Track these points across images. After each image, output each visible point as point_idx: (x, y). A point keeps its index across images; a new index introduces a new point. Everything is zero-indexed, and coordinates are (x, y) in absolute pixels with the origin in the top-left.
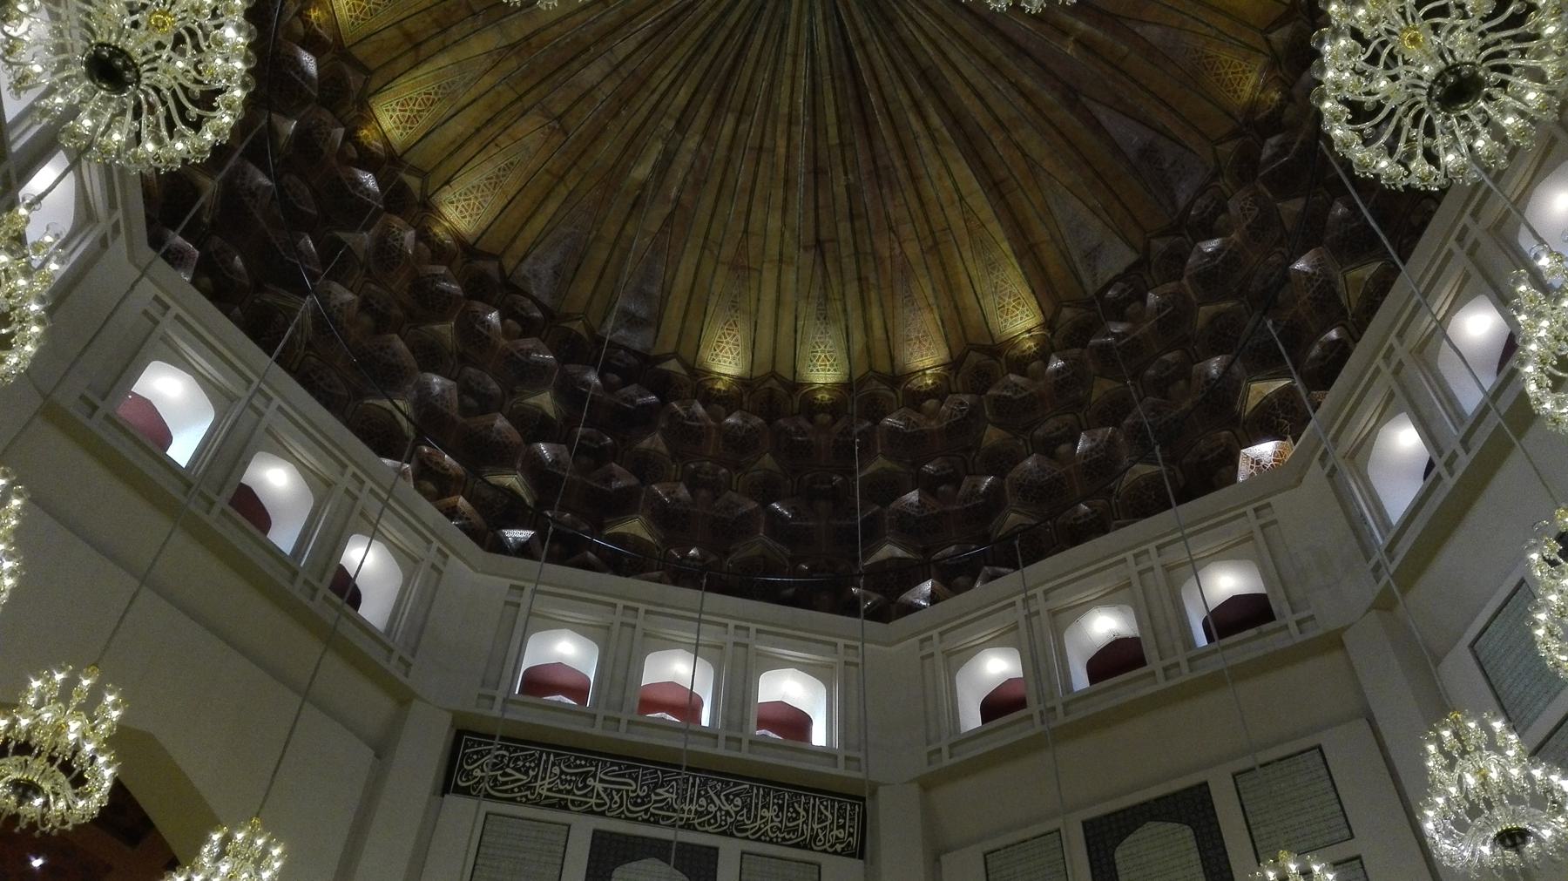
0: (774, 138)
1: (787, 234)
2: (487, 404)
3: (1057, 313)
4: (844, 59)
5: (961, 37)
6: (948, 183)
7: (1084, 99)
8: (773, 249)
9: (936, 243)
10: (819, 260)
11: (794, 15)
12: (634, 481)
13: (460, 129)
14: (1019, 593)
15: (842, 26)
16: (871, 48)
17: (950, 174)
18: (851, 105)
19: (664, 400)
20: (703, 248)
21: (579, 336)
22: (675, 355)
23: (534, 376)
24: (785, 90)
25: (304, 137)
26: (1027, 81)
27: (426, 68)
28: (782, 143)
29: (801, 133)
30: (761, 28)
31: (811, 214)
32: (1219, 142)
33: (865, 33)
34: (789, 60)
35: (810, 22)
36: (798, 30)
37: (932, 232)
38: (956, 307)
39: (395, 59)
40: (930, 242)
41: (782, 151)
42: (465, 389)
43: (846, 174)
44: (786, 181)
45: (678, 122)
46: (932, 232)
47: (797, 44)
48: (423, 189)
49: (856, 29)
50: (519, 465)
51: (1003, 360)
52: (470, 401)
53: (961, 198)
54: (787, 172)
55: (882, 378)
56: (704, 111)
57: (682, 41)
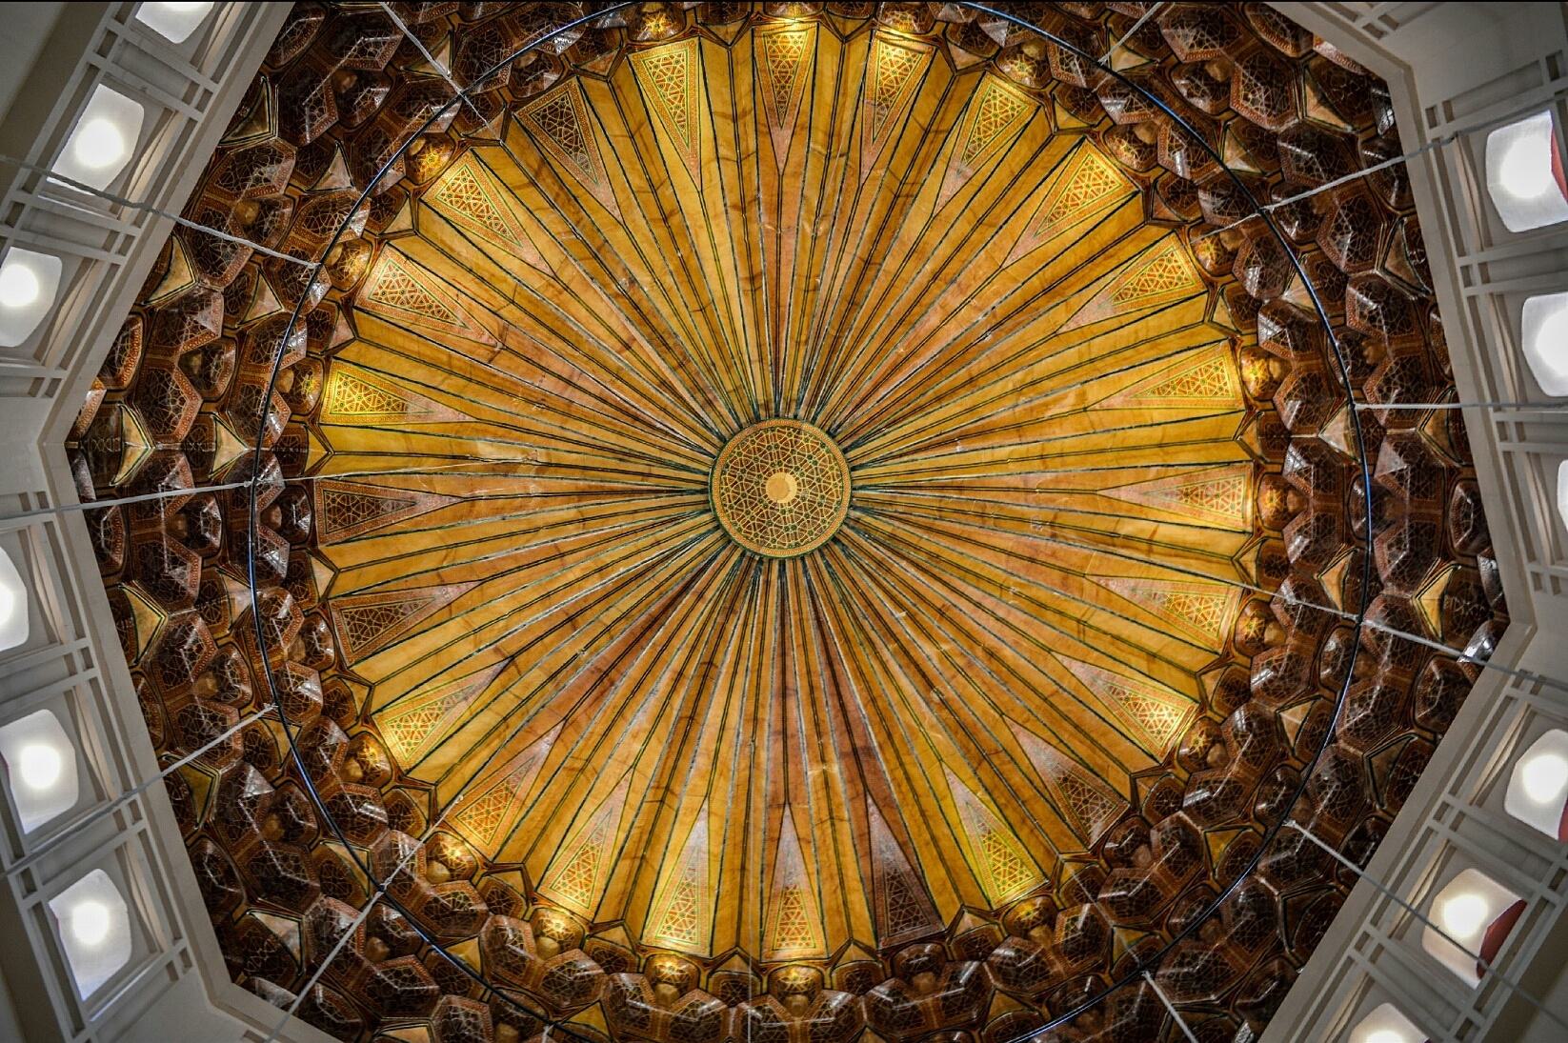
0: (577, 562)
1: (502, 623)
2: (203, 381)
3: (609, 925)
4: (677, 589)
5: (759, 676)
6: (637, 747)
7: (787, 812)
8: (478, 620)
9: (582, 770)
10: (498, 667)
11: (689, 523)
12: (194, 593)
13: (464, 253)
14: (1505, 680)
15: (703, 570)
16: (701, 606)
17: (646, 742)
18: (643, 618)
19: (286, 584)
20: (448, 547)
21: (304, 457)
22: (337, 571)
23: (252, 426)
24: (622, 551)
25: (434, 90)
26: (763, 755)
27: (512, 202)
28: (577, 573)
29: (594, 586)
30: (664, 500)
31: (532, 638)
32: (856, 943)
33: (709, 594)
34: (651, 540)
35: (693, 540)
36: (679, 535)
37: (588, 760)
38: (544, 829)
39: (518, 165)
40: (578, 765)
41: (571, 577)
42: (210, 352)
43: (587, 647)
44: (548, 595)
45: (549, 465)
46: (588, 760)
47: (666, 540)
48: (400, 234)
49: (708, 585)
50: (160, 446)
51: (532, 909)
52: (197, 361)
53: (634, 766)
54: (556, 591)
55: (433, 803)
56: (566, 485)
57: (620, 434)
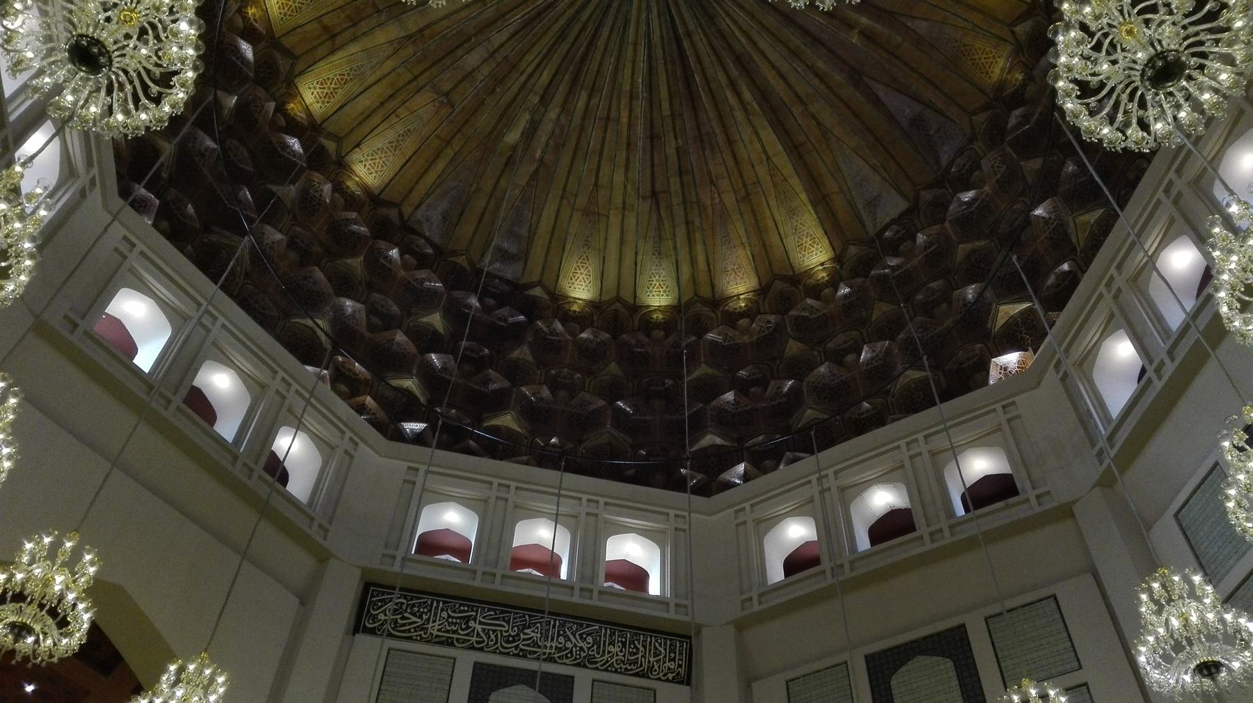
0: (618, 110)
1: (629, 187)
2: (389, 323)
3: (844, 250)
4: (674, 47)
5: (768, 30)
6: (758, 146)
7: (866, 79)
8: (618, 199)
9: (748, 194)
10: (654, 207)
11: (634, 12)
12: (506, 384)
13: (368, 103)
14: (814, 473)
15: (673, 21)
16: (696, 38)
17: (760, 139)
18: (680, 84)
19: (531, 319)
20: (562, 198)
21: (463, 268)
22: (540, 283)
23: (426, 300)
24: (627, 72)
25: (243, 109)
26: (821, 65)
27: (341, 54)
28: (625, 114)
29: (640, 106)
30: (609, 22)
31: (648, 171)
32: (974, 113)
33: (692, 26)
34: (630, 48)
35: (648, 18)
36: (638, 24)
37: (745, 185)
38: (764, 245)
39: (315, 47)
40: (743, 193)
41: (625, 120)
42: (372, 310)
43: (676, 139)
44: (628, 145)
45: (542, 97)
46: (745, 185)
47: (637, 35)
48: (338, 151)
49: (684, 23)
50: (415, 371)
51: (801, 288)
52: (376, 320)
53: (768, 158)
54: (629, 137)
55: (705, 302)
56: (563, 89)
57: (545, 33)
